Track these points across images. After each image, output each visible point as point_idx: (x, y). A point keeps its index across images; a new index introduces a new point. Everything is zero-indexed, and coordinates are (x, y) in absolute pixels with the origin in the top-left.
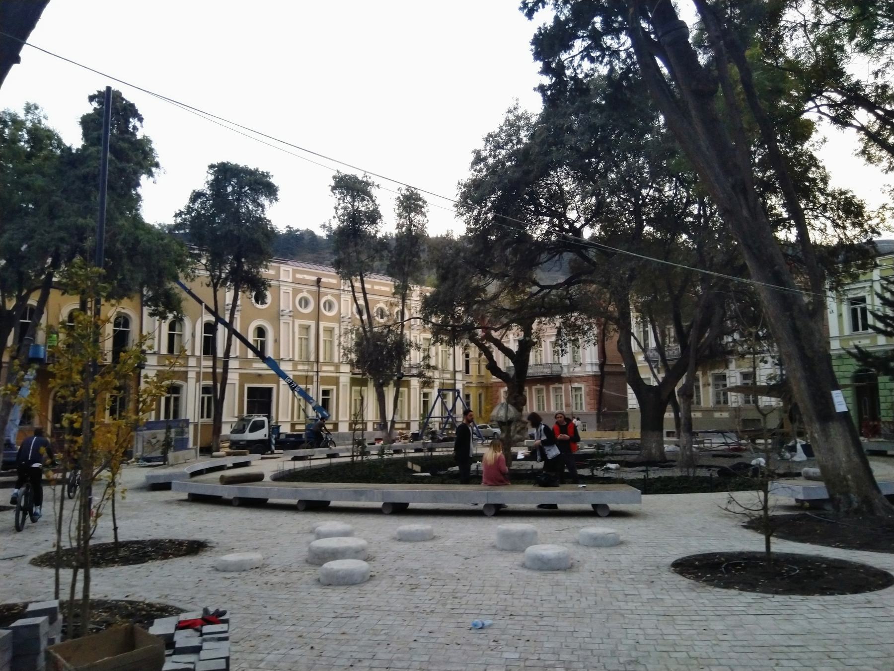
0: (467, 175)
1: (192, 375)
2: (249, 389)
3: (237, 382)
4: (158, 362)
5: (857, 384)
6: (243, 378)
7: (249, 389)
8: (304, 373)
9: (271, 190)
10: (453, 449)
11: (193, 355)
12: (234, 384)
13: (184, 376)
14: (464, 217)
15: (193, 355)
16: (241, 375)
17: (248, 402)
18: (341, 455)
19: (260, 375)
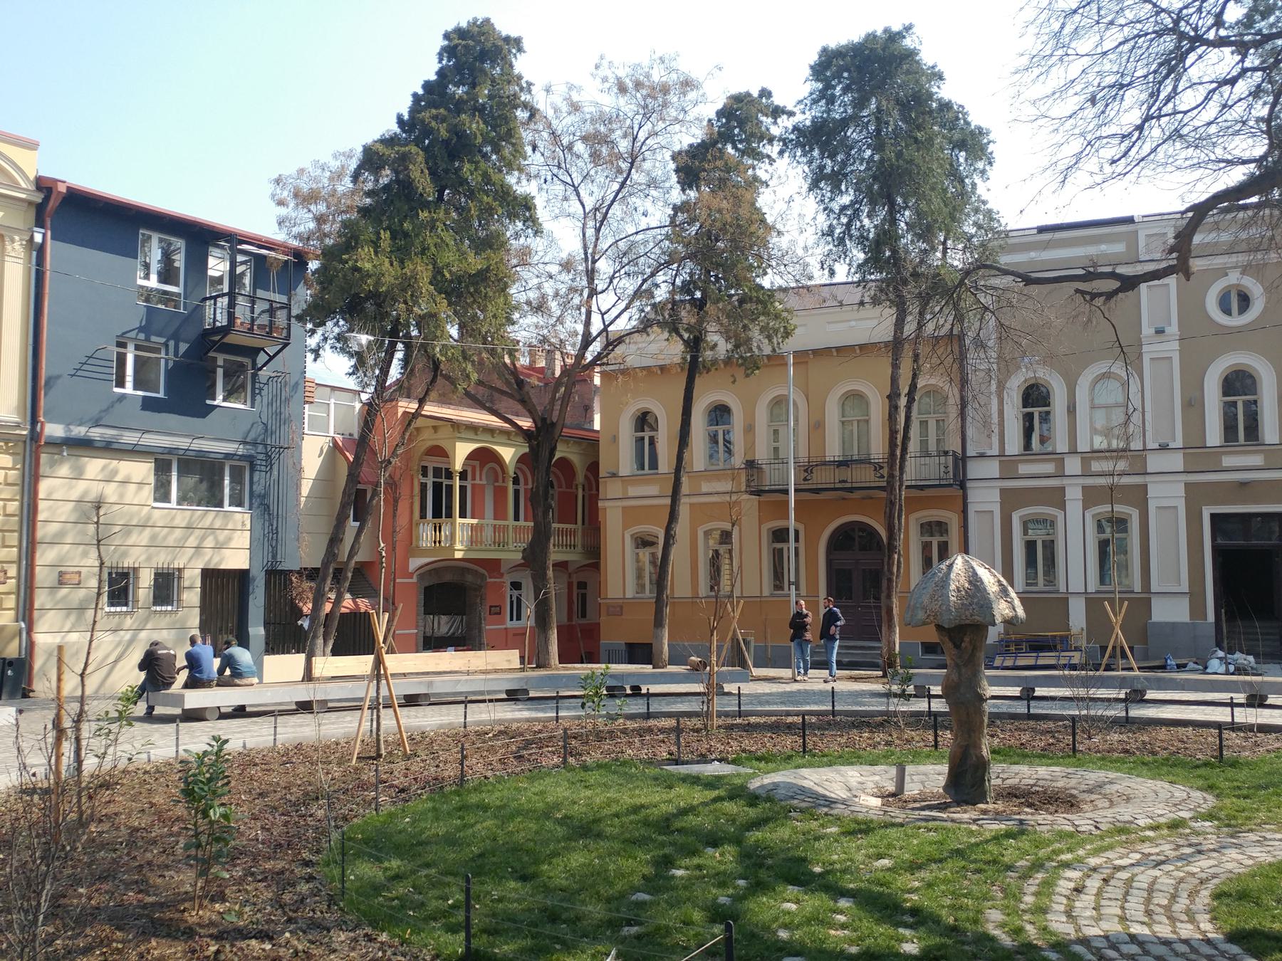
0: (464, 25)
1: (1074, 494)
2: (1213, 516)
3: (997, 509)
4: (1001, 471)
5: (257, 631)
6: (1195, 495)
7: (1213, 516)
8: (1109, 480)
9: (940, 77)
10: (989, 707)
11: (1073, 451)
12: (1176, 507)
13: (1057, 498)
14: (283, 211)
15: (1073, 451)
16: (1003, 492)
17: (1216, 550)
18: (1150, 695)
19: (1243, 484)
